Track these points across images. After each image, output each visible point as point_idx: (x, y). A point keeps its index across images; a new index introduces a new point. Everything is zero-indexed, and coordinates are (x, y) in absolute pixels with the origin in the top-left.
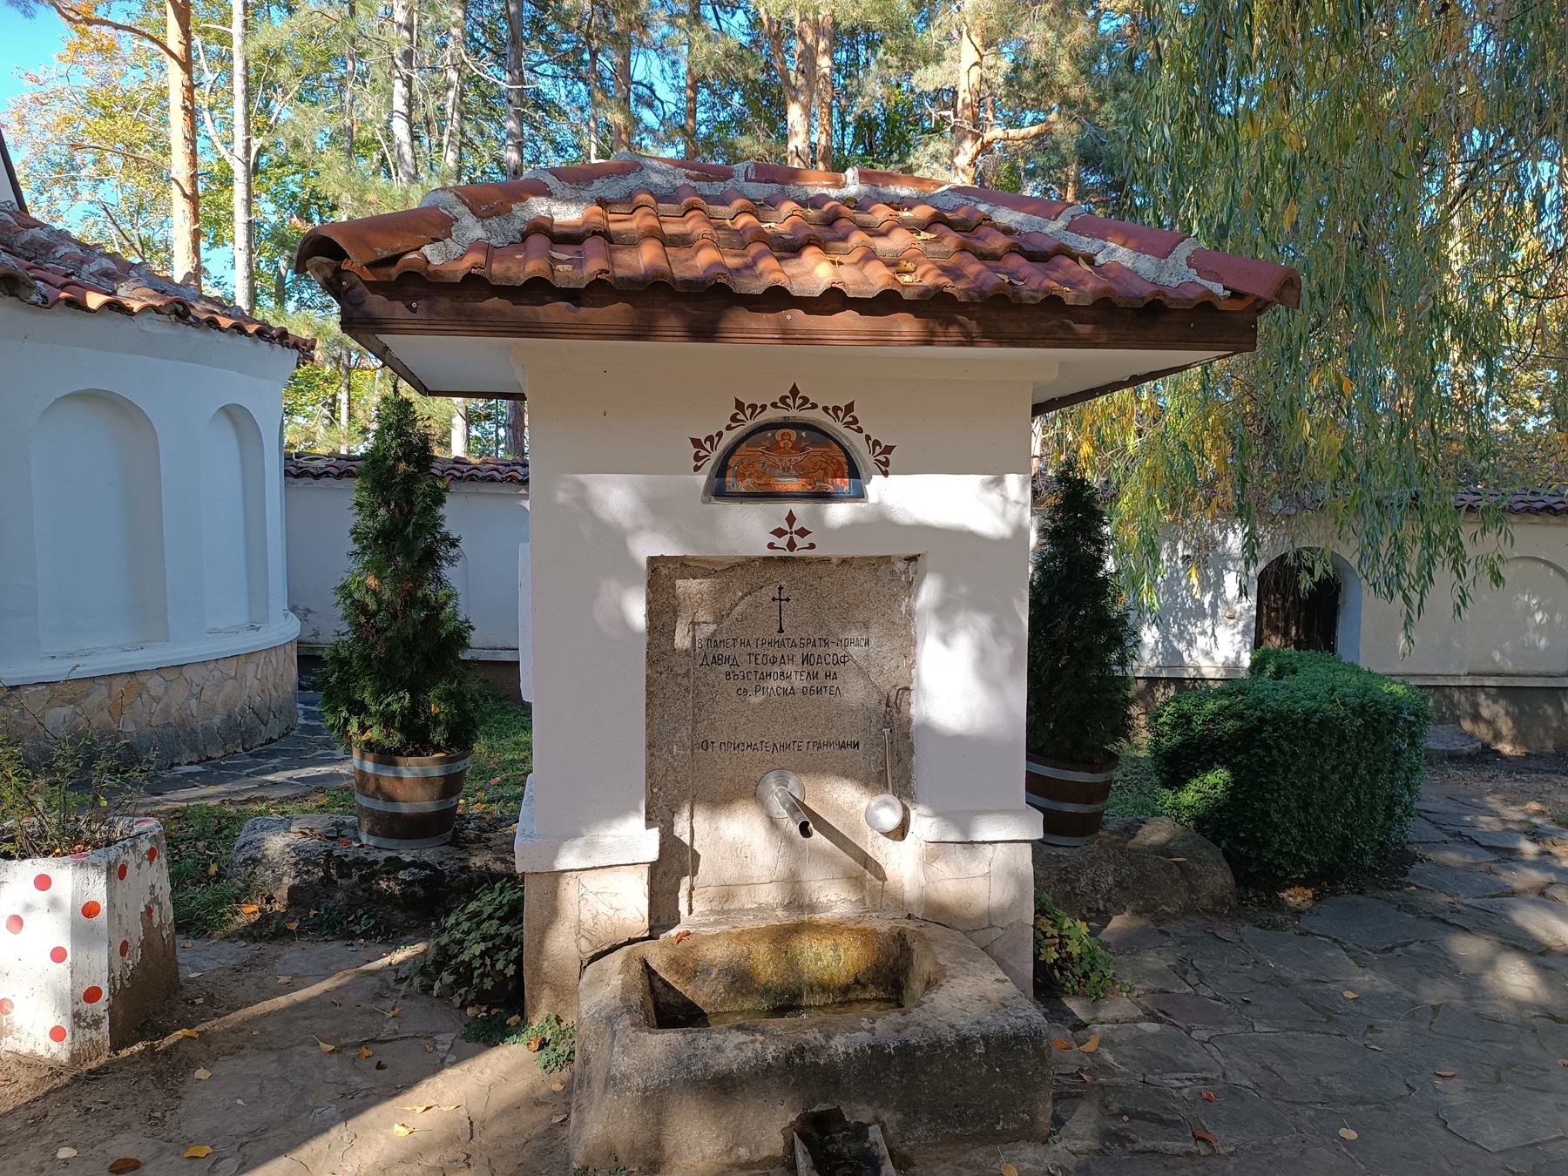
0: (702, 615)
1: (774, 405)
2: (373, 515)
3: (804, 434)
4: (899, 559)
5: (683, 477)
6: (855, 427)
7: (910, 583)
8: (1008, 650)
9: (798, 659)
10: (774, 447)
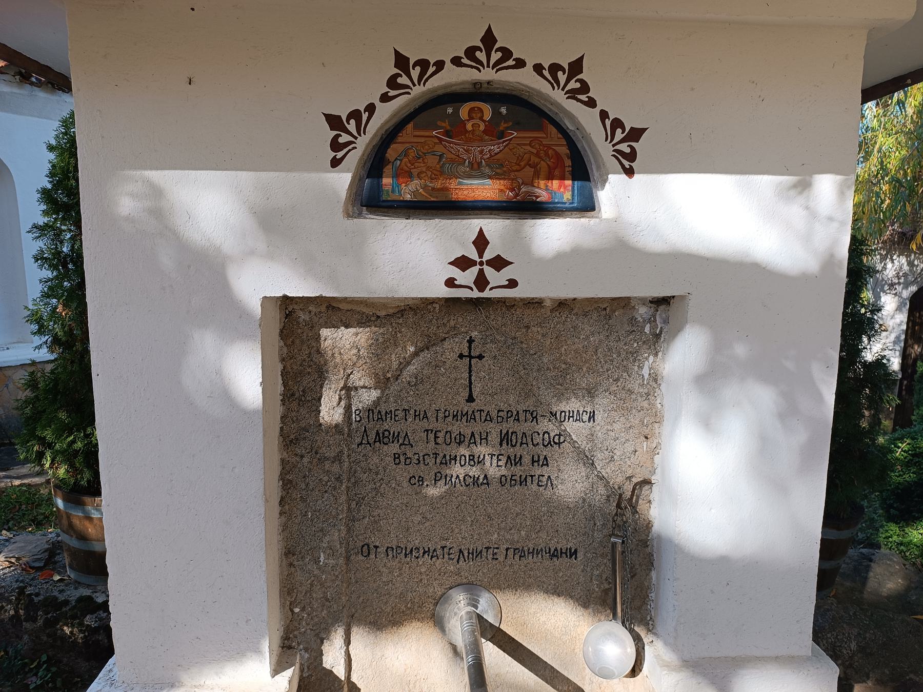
0: (359, 378)
1: (456, 61)
3: (503, 110)
4: (643, 301)
5: (314, 176)
6: (583, 97)
7: (657, 336)
8: (801, 436)
9: (494, 437)
10: (456, 130)
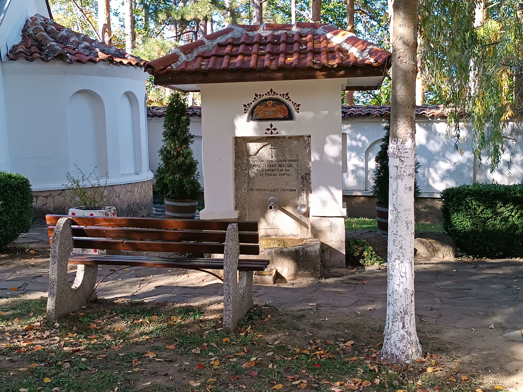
1: (266, 94)
2: (170, 128)
10: (266, 106)
